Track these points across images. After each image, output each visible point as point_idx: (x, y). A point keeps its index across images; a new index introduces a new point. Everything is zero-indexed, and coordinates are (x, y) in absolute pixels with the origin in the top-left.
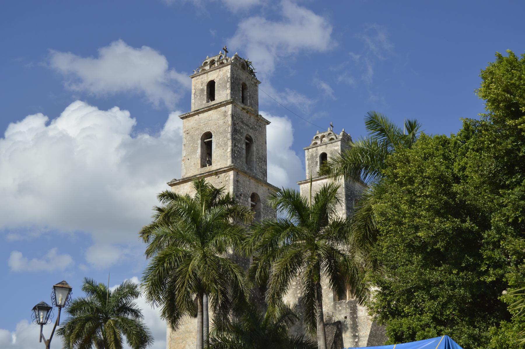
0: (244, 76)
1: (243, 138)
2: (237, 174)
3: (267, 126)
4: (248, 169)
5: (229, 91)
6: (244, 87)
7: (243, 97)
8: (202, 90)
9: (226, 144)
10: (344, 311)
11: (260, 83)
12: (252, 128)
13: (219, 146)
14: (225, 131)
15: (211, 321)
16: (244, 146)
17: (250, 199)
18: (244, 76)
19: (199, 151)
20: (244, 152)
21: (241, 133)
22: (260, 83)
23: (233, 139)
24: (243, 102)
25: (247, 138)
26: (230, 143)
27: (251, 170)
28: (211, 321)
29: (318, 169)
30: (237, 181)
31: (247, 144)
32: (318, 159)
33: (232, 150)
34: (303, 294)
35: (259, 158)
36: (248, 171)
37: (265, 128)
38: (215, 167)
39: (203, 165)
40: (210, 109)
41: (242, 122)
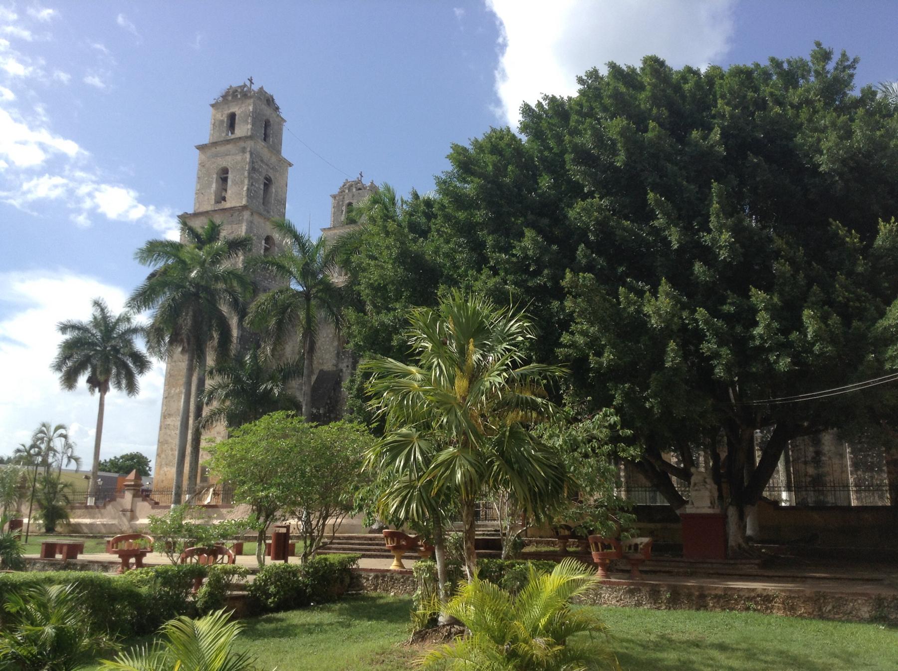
0: (268, 111)
1: (262, 178)
2: (252, 214)
3: (290, 168)
4: (265, 210)
5: (250, 126)
6: (267, 124)
7: (265, 134)
8: (222, 122)
9: (242, 182)
10: (346, 360)
11: (285, 121)
12: (272, 169)
13: (235, 183)
14: (243, 169)
15: (823, 575)
16: (262, 187)
17: (263, 242)
18: (268, 111)
19: (214, 186)
20: (262, 192)
21: (260, 173)
22: (285, 121)
23: (250, 178)
24: (265, 140)
25: (266, 179)
26: (246, 182)
27: (268, 212)
28: (823, 575)
29: (343, 218)
30: (251, 222)
31: (265, 184)
32: (344, 208)
33: (248, 189)
34: (22, 469)
35: (278, 200)
36: (265, 213)
37: (287, 170)
38: (228, 205)
39: (218, 202)
40: (228, 142)
41: (262, 161)
